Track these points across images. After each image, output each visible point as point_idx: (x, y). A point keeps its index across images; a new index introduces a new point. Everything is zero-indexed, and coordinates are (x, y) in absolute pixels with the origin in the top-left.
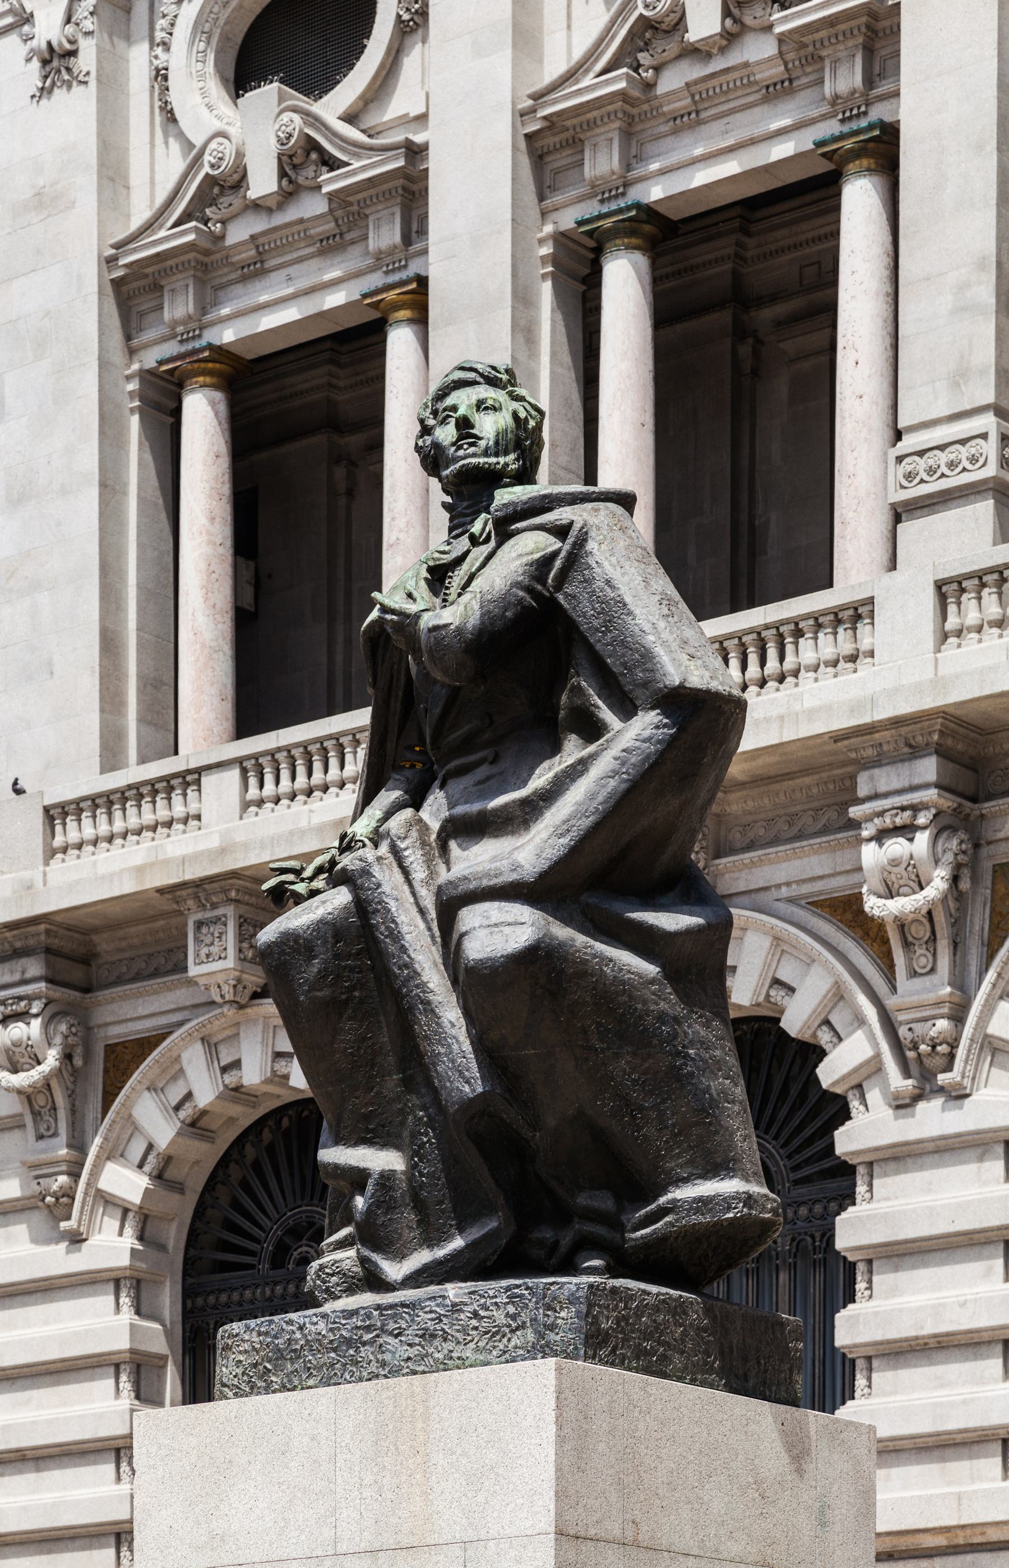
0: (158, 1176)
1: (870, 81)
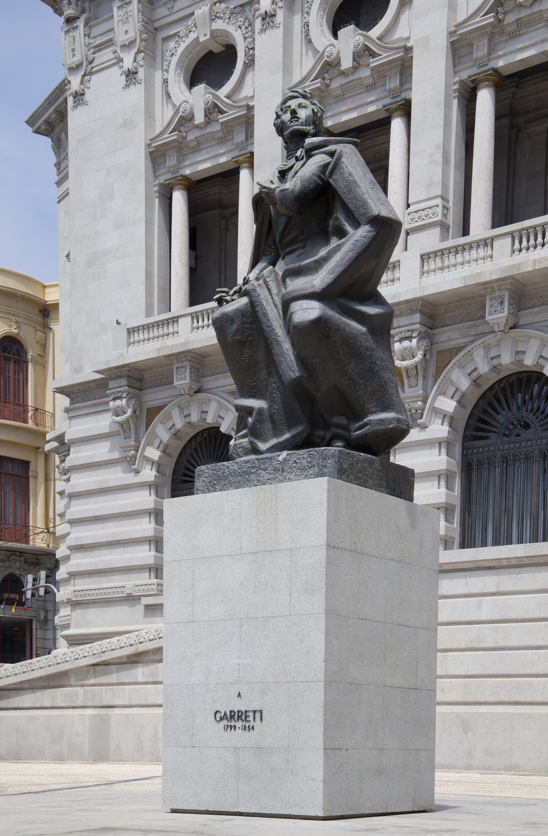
0: (164, 452)
1: (401, 84)
